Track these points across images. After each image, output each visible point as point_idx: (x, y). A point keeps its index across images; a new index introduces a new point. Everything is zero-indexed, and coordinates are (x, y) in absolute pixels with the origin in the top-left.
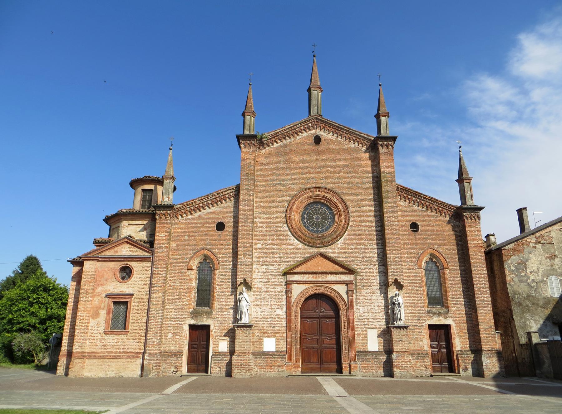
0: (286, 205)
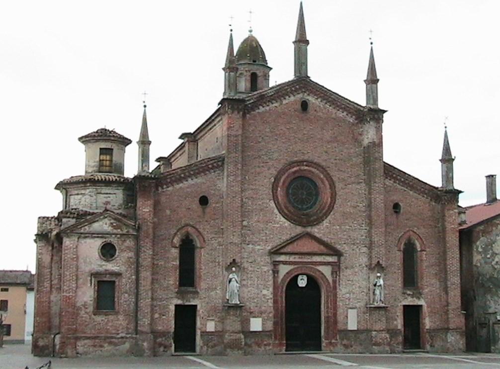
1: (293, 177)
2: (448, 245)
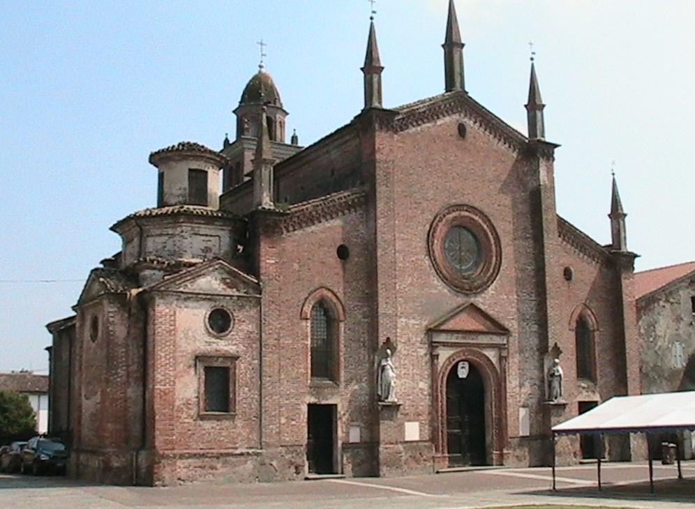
0: (428, 227)
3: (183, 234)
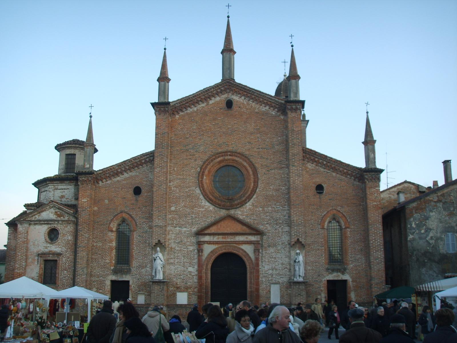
1: (218, 167)
2: (370, 221)
3: (50, 190)
